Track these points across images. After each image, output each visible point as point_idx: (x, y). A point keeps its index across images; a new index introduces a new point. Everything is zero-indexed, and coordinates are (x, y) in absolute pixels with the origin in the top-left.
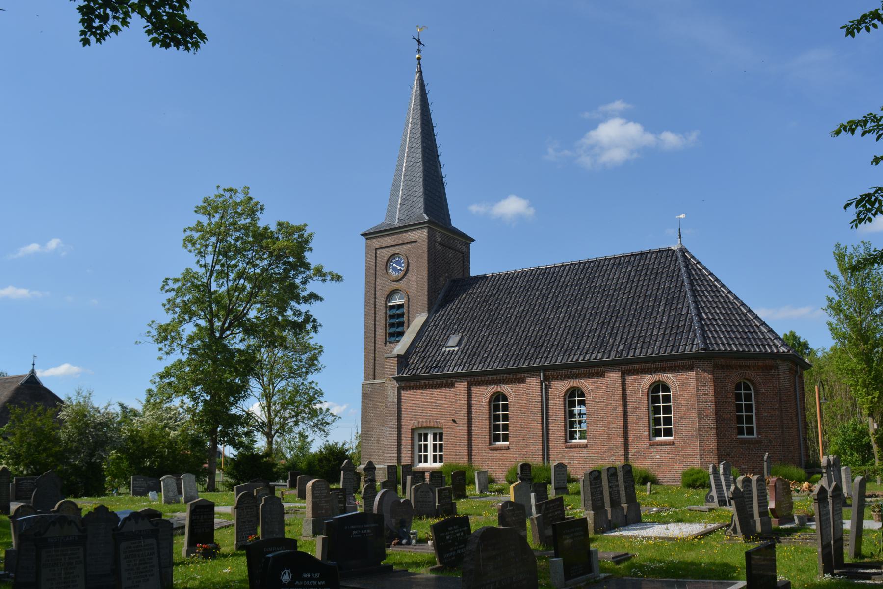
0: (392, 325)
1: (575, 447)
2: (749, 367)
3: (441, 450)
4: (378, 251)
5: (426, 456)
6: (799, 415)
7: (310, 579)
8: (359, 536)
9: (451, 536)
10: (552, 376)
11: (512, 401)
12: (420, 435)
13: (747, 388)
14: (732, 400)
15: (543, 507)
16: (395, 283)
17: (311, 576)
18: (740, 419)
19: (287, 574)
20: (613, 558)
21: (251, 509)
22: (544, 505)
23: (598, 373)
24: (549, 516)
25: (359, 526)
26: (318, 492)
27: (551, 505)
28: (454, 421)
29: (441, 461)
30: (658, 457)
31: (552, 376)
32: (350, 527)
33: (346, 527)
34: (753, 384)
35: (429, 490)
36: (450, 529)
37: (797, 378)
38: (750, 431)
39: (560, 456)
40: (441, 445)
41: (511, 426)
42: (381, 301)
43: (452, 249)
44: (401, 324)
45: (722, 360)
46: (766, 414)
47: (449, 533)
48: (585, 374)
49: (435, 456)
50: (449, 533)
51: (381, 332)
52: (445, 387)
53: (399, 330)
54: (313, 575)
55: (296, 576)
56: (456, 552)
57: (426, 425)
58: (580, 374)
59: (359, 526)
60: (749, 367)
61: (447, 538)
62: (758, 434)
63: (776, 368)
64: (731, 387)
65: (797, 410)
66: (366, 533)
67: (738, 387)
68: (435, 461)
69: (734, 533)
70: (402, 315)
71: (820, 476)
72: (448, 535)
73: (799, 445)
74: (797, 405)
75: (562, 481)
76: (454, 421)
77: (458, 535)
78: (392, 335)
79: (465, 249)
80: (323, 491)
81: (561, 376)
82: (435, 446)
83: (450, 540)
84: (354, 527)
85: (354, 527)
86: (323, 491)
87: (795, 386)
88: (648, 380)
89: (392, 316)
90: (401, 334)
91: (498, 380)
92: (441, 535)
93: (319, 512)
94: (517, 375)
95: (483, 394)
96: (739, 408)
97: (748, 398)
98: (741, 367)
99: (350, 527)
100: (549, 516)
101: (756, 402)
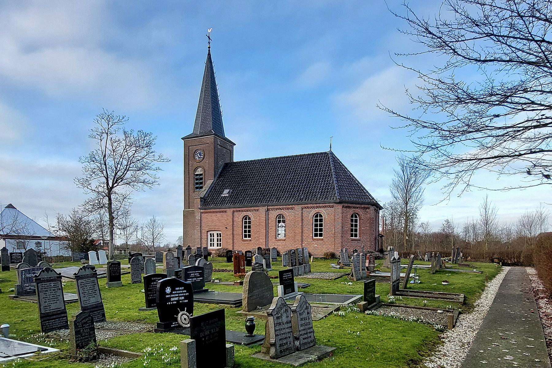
11: (252, 219)
12: (211, 234)
13: (356, 217)
18: (352, 230)
23: (291, 208)
25: (193, 272)
55: (173, 289)
59: (193, 272)
64: (349, 216)
84: (192, 272)
85: (192, 272)
96: (352, 225)
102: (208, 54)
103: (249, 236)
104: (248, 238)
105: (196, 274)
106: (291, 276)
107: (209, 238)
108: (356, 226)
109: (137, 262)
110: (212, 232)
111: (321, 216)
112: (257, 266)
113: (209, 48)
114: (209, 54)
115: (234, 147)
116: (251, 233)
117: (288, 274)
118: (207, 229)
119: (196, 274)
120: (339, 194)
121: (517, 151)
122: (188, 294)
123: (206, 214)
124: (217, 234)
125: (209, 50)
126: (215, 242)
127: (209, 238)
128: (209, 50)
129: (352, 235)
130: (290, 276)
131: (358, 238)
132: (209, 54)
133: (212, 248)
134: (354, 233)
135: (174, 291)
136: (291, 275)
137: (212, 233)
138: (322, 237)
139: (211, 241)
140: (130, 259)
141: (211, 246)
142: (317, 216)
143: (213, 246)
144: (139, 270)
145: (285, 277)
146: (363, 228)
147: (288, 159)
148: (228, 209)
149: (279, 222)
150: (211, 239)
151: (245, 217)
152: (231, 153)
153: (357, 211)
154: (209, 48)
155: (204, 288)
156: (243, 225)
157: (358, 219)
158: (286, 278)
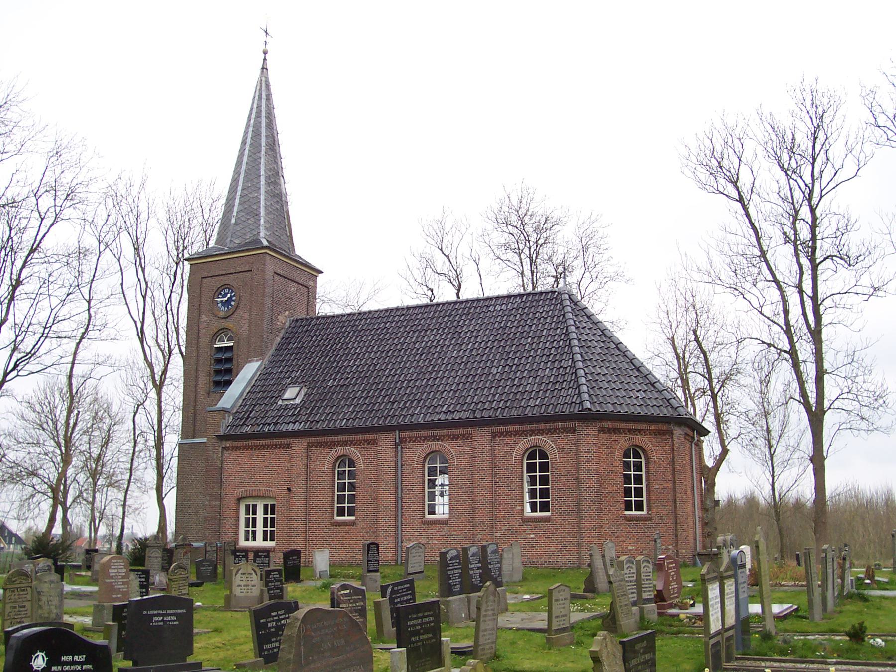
0: (218, 372)
1: (435, 524)
2: (640, 431)
3: (272, 526)
4: (205, 280)
5: (254, 532)
6: (695, 489)
7: (74, 663)
8: (161, 623)
9: (274, 623)
10: (409, 437)
11: (360, 465)
12: (248, 507)
13: (637, 456)
14: (620, 470)
15: (389, 590)
16: (224, 320)
17: (73, 658)
18: (627, 492)
19: (40, 658)
20: (452, 648)
21: (24, 591)
22: (391, 587)
23: (464, 435)
24: (396, 601)
25: (161, 612)
26: (114, 571)
27: (399, 588)
28: (289, 490)
29: (272, 539)
30: (532, 536)
31: (409, 437)
32: (151, 612)
33: (145, 612)
34: (643, 450)
35: (253, 572)
36: (273, 614)
37: (693, 445)
38: (639, 507)
39: (416, 534)
40: (273, 519)
41: (359, 497)
42: (204, 340)
43: (295, 282)
44: (229, 371)
45: (609, 423)
46: (657, 487)
47: (272, 619)
48: (449, 436)
49: (265, 532)
50: (272, 619)
51: (204, 380)
52: (267, 449)
53: (226, 378)
54: (76, 658)
55: (53, 660)
56: (163, 619)
57: (255, 494)
58: (443, 436)
59: (161, 612)
60: (640, 431)
61: (270, 625)
62: (649, 509)
63: (671, 433)
64: (618, 454)
65: (693, 483)
66: (169, 621)
67: (626, 455)
68: (265, 539)
69: (613, 624)
70: (230, 360)
71: (8, 542)
72: (270, 622)
73: (695, 523)
74: (693, 476)
75: (418, 565)
76: (289, 490)
77: (283, 622)
78: (217, 384)
79: (311, 283)
80: (120, 571)
81: (420, 437)
82: (265, 520)
83: (273, 627)
84: (155, 612)
85: (155, 612)
86: (120, 571)
87: (692, 455)
88: (523, 444)
89: (218, 361)
90: (228, 383)
91: (344, 441)
92: (262, 621)
93: (114, 596)
94: (367, 436)
95: (325, 459)
96: (627, 479)
97: (638, 467)
98: (630, 430)
99: (151, 612)
100: (396, 601)
101: (647, 472)
102: (261, 67)
103: (351, 512)
104: (346, 518)
105: (169, 618)
106: (432, 622)
107: (243, 516)
108: (638, 479)
109: (21, 583)
110: (251, 502)
111: (543, 455)
112: (346, 595)
113: (265, 53)
114: (264, 68)
115: (320, 279)
116: (358, 505)
117: (424, 617)
118: (239, 492)
119: (169, 618)
120: (590, 396)
121: (174, 414)
122: (89, 666)
123: (234, 453)
124: (266, 507)
125: (265, 59)
126: (260, 528)
127: (243, 516)
128: (265, 59)
129: (628, 506)
130: (430, 622)
131: (644, 512)
132: (264, 68)
133: (251, 543)
134: (633, 499)
135: (57, 665)
136: (431, 619)
137: (251, 503)
138: (644, 512)
139: (247, 526)
140: (10, 580)
141: (247, 539)
142: (532, 456)
143: (254, 539)
144: (24, 607)
145: (414, 625)
146: (657, 487)
147: (445, 307)
148: (296, 440)
149: (432, 472)
150: (247, 520)
151: (342, 460)
152: (310, 293)
153: (640, 440)
154: (265, 53)
155: (190, 660)
156: (333, 481)
157: (643, 460)
158: (417, 627)
